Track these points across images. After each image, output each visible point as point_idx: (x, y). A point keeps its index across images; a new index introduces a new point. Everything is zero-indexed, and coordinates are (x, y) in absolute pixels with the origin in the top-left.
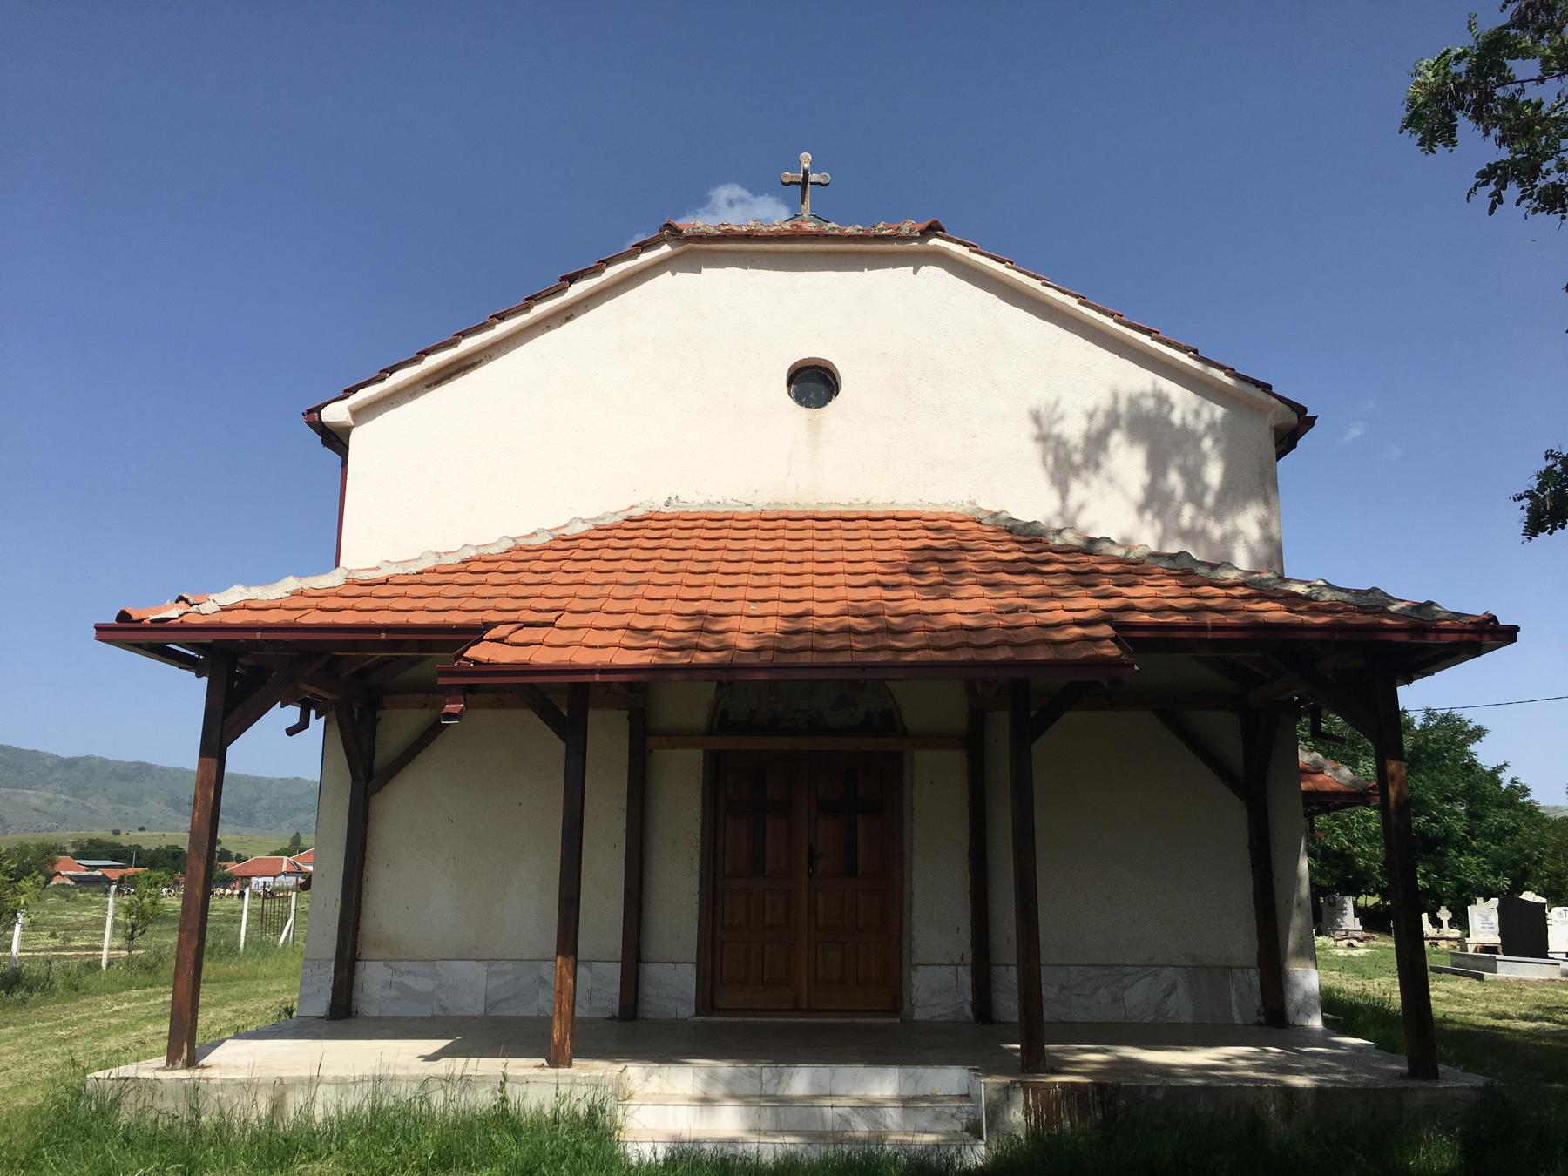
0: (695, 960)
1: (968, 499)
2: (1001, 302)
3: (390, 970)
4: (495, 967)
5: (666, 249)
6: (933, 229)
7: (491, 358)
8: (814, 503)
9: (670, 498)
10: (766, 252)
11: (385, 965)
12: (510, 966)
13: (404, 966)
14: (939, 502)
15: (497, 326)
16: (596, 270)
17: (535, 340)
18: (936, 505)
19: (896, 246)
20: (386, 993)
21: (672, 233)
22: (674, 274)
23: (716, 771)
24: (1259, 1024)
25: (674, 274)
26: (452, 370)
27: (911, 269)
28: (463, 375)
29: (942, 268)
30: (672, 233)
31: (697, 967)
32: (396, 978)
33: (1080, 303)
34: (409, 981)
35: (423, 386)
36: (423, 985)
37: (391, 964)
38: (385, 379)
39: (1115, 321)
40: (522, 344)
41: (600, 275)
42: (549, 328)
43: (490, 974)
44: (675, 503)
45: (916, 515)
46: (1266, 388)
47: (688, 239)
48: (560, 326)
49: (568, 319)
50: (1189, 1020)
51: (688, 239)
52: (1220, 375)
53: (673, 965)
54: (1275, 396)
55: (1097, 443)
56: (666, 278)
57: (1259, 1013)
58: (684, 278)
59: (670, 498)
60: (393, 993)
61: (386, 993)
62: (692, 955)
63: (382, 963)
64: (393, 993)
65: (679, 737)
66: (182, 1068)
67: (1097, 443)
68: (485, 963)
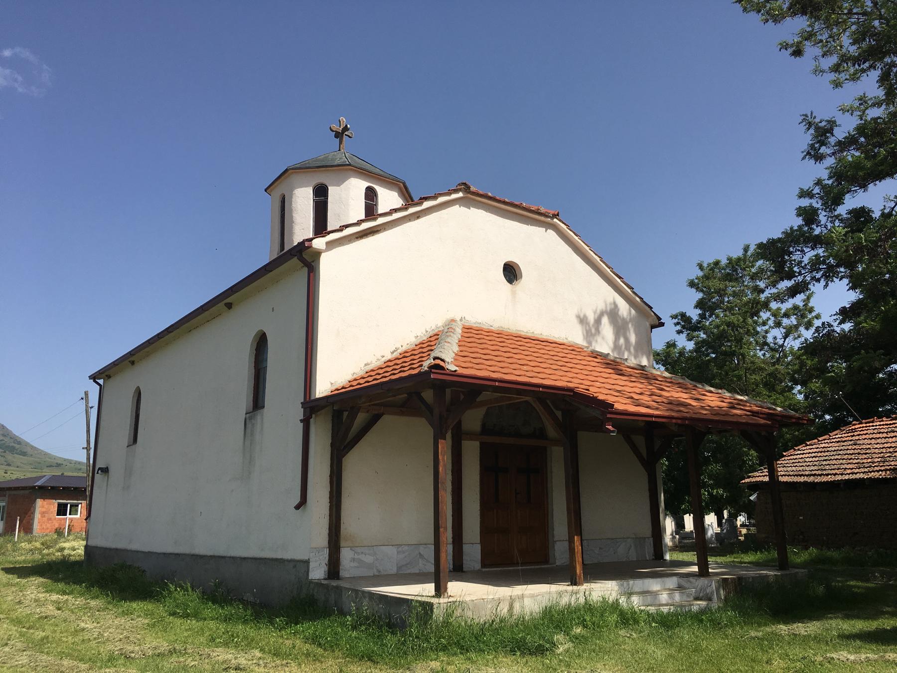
0: (433, 543)
1: (565, 337)
2: (573, 252)
3: (353, 552)
4: (400, 549)
5: (460, 195)
6: (556, 216)
7: (385, 230)
8: (514, 329)
9: (462, 317)
10: (517, 214)
11: (351, 549)
12: (406, 548)
13: (359, 550)
14: (556, 337)
15: (393, 214)
16: (435, 197)
17: (405, 225)
18: (555, 337)
19: (542, 218)
20: (352, 564)
21: (466, 188)
22: (460, 207)
23: (485, 450)
24: (653, 559)
25: (460, 207)
26: (368, 231)
27: (544, 229)
28: (373, 235)
29: (555, 232)
30: (466, 188)
31: (481, 546)
32: (356, 556)
33: (600, 260)
34: (362, 557)
35: (355, 237)
36: (369, 559)
37: (353, 549)
38: (343, 230)
39: (611, 271)
40: (398, 226)
41: (436, 200)
42: (410, 220)
43: (398, 552)
44: (464, 320)
45: (538, 339)
46: (651, 308)
47: (474, 193)
48: (415, 220)
49: (418, 217)
50: (635, 559)
51: (474, 193)
52: (638, 299)
53: (471, 545)
54: (652, 311)
55: (598, 321)
56: (456, 208)
57: (653, 555)
58: (463, 209)
59: (462, 317)
60: (356, 564)
61: (352, 564)
62: (478, 540)
63: (349, 548)
64: (356, 564)
65: (472, 436)
66: (678, 582)
67: (598, 321)
68: (396, 546)
